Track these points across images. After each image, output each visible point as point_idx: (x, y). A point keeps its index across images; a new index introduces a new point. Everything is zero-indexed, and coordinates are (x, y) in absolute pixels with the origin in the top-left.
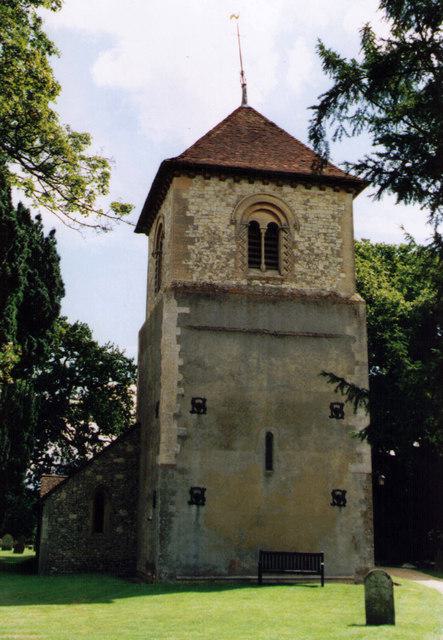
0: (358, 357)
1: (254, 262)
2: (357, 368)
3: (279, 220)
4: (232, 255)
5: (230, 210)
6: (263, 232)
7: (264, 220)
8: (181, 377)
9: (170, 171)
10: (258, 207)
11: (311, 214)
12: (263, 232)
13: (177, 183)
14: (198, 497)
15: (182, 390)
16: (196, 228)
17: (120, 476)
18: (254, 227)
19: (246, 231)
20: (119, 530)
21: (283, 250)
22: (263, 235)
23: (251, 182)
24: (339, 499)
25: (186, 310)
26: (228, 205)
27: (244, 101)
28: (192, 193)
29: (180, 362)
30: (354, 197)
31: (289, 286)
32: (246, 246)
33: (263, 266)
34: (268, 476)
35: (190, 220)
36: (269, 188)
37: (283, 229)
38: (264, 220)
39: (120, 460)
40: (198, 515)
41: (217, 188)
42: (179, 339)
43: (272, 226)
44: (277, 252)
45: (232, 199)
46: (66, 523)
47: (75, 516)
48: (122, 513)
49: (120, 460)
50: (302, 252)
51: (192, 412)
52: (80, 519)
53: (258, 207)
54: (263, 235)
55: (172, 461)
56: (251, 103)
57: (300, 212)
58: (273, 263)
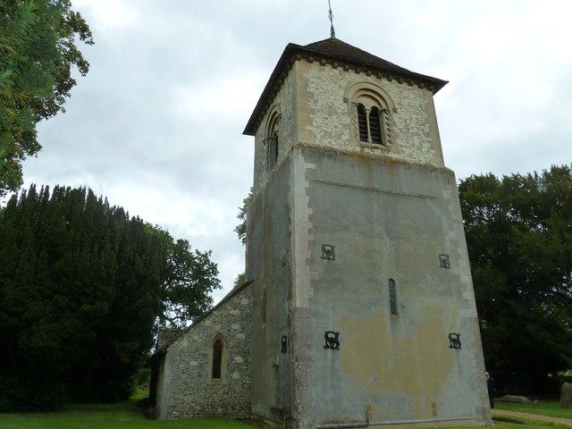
0: (454, 217)
1: (364, 138)
2: (455, 225)
3: (380, 104)
4: (345, 126)
5: (342, 92)
6: (368, 113)
7: (369, 104)
8: (311, 225)
9: (293, 54)
10: (363, 93)
11: (405, 102)
12: (368, 113)
13: (299, 65)
14: (332, 342)
15: (312, 237)
16: (316, 102)
17: (235, 326)
18: (361, 108)
19: (356, 108)
20: (236, 375)
21: (386, 127)
22: (368, 115)
23: (357, 72)
24: (455, 343)
25: (312, 166)
26: (340, 87)
27: (333, 33)
28: (311, 74)
29: (310, 212)
30: (434, 93)
31: (393, 156)
32: (357, 120)
33: (370, 139)
34: (393, 321)
35: (311, 95)
36: (372, 79)
37: (384, 111)
38: (369, 104)
39: (236, 312)
40: (333, 360)
41: (331, 73)
42: (309, 191)
43: (374, 109)
44: (379, 131)
45: (343, 83)
46: (187, 369)
47: (196, 364)
48: (239, 359)
49: (236, 312)
50: (401, 130)
51: (323, 258)
52: (201, 366)
53: (363, 93)
54: (368, 115)
55: (306, 305)
56: (337, 36)
57: (396, 100)
58: (378, 138)
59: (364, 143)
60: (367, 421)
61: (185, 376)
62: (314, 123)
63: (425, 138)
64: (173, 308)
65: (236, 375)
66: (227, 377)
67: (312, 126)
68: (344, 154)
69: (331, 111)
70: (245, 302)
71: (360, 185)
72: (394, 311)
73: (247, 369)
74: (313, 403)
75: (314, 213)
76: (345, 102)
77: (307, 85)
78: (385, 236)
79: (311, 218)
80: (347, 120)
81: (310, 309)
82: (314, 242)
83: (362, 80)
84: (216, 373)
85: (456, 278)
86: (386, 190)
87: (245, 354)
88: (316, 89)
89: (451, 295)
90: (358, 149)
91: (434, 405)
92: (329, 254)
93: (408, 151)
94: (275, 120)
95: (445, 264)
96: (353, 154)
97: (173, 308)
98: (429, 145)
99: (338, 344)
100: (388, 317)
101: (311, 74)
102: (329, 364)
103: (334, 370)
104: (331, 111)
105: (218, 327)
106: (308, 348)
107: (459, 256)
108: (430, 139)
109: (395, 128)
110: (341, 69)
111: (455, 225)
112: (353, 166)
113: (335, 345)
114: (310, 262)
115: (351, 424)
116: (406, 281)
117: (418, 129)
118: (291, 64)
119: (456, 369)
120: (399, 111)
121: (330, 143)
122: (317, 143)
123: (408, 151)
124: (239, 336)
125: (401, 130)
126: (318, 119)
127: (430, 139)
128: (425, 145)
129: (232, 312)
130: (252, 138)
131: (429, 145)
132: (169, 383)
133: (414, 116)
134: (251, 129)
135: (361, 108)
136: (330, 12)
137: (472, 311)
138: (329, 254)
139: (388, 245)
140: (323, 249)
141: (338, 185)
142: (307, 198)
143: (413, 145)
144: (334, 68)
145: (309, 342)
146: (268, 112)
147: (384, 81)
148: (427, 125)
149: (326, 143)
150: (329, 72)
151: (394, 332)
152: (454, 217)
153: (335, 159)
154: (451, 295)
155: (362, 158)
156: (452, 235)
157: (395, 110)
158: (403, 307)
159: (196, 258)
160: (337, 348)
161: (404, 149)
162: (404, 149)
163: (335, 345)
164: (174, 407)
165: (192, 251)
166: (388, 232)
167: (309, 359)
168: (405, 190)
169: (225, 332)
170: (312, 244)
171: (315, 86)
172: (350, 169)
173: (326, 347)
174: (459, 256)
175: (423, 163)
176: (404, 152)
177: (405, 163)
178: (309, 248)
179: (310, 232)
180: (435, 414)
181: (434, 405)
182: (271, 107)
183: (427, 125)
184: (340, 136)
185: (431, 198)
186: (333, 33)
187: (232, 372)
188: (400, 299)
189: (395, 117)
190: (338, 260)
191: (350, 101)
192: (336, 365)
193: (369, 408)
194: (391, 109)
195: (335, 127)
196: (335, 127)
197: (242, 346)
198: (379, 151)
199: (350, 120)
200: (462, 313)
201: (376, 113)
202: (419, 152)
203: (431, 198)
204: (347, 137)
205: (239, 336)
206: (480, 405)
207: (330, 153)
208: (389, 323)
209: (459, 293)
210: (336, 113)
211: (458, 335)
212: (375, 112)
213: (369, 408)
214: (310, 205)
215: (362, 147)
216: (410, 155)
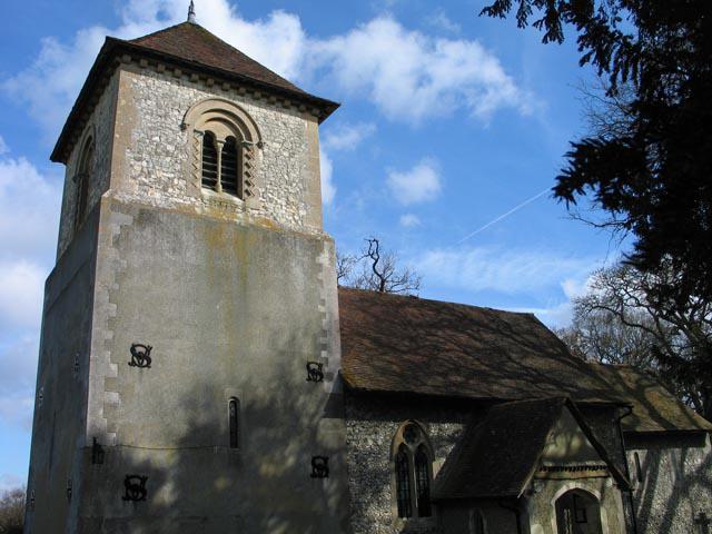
7: (222, 133)
18: (209, 138)
19: (201, 139)
27: (191, 12)
38: (222, 133)
56: (199, 20)
58: (233, 186)
94: (89, 147)
99: (149, 361)
113: (145, 362)
118: (115, 66)
130: (61, 168)
134: (60, 154)
135: (209, 138)
146: (84, 132)
157: (260, 145)
160: (148, 366)
163: (145, 362)
173: (132, 364)
186: (191, 12)
199: (258, 163)
201: (233, 147)
211: (149, 349)
212: (233, 147)
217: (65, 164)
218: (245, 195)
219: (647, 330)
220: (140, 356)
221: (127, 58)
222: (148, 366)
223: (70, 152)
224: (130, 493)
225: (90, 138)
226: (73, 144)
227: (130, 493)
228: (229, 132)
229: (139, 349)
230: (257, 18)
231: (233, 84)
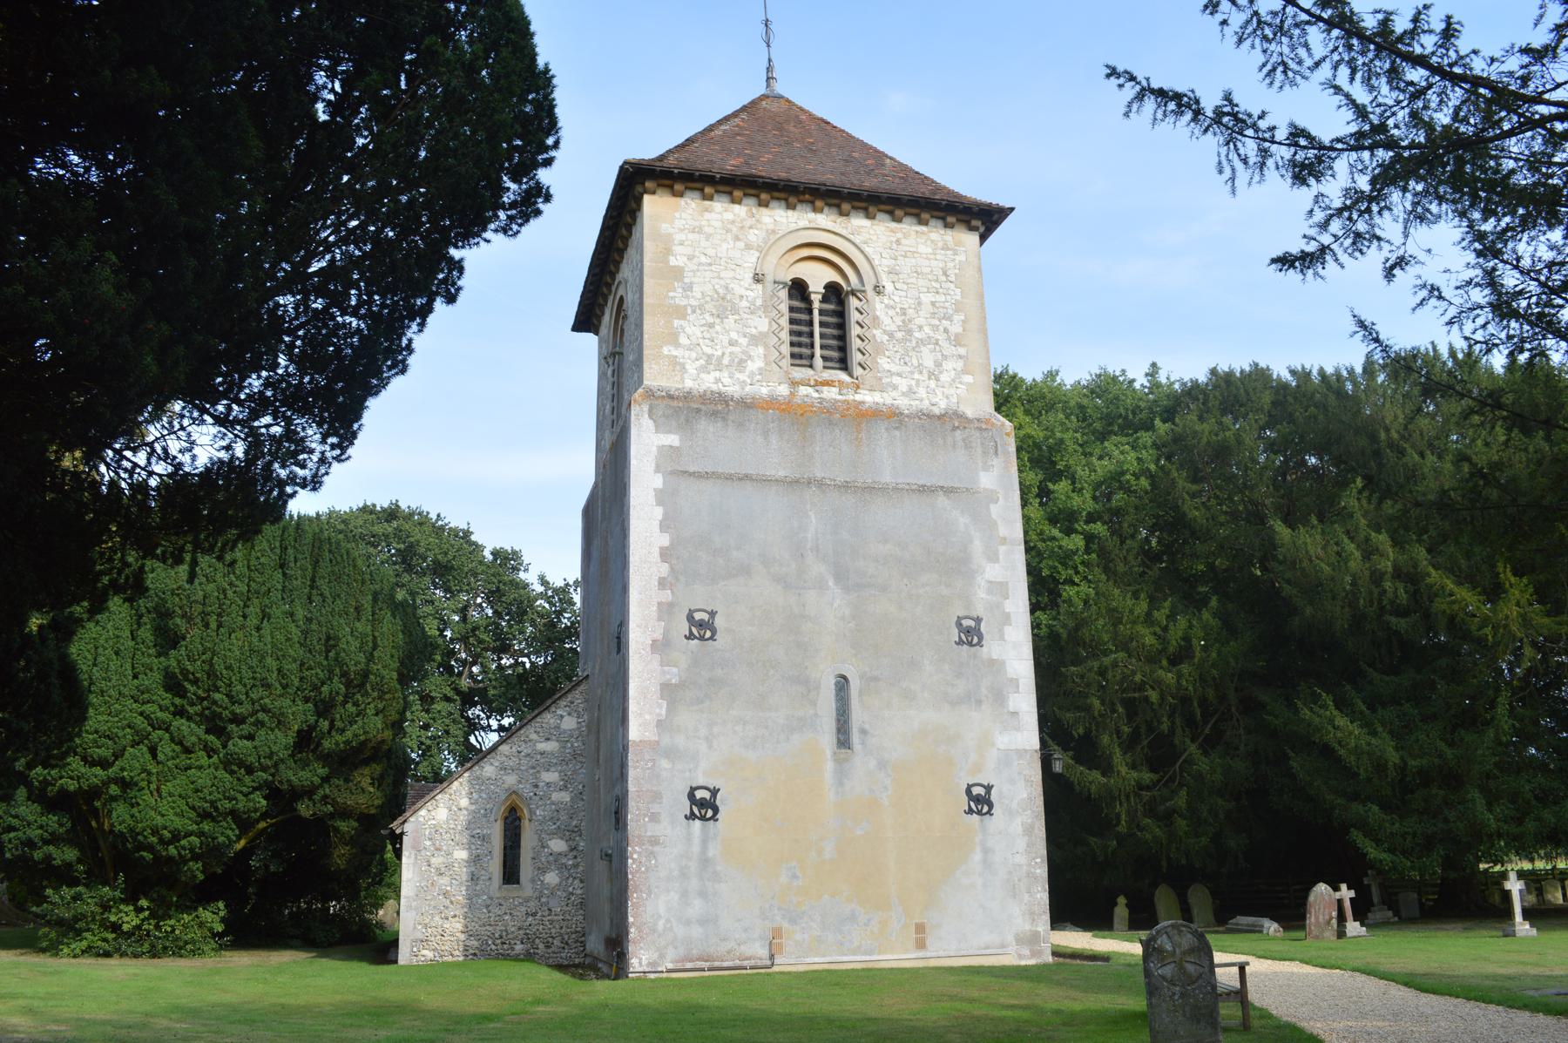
0: (1003, 531)
1: (801, 354)
2: (1002, 549)
4: (755, 340)
5: (751, 259)
6: (816, 299)
7: (818, 278)
11: (906, 265)
13: (655, 207)
14: (704, 806)
15: (667, 596)
16: (689, 288)
17: (551, 776)
18: (798, 289)
20: (552, 878)
24: (981, 802)
25: (673, 440)
26: (748, 247)
29: (665, 540)
31: (867, 397)
33: (818, 362)
34: (838, 761)
35: (678, 273)
37: (853, 293)
38: (818, 278)
40: (705, 842)
42: (661, 497)
45: (754, 236)
46: (449, 866)
48: (558, 845)
50: (891, 335)
55: (651, 735)
56: (780, 88)
57: (883, 264)
59: (800, 373)
60: (772, 957)
61: (444, 881)
62: (683, 340)
63: (949, 349)
64: (494, 724)
65: (552, 878)
66: (533, 881)
67: (677, 345)
68: (747, 405)
69: (724, 306)
70: (569, 723)
71: (782, 473)
72: (843, 738)
73: (576, 866)
74: (661, 925)
75: (672, 544)
76: (758, 281)
77: (668, 251)
78: (831, 583)
79: (665, 554)
80: (761, 324)
81: (658, 743)
82: (671, 605)
83: (802, 224)
84: (511, 874)
85: (996, 666)
86: (841, 479)
87: (570, 833)
88: (691, 258)
89: (1452, 619)
90: (783, 390)
91: (920, 928)
92: (702, 628)
93: (903, 384)
95: (971, 635)
96: (771, 403)
97: (494, 724)
98: (960, 365)
100: (829, 753)
101: (679, 223)
102: (696, 848)
103: (705, 862)
104: (724, 306)
105: (511, 780)
106: (650, 821)
107: (1007, 619)
108: (962, 351)
109: (877, 333)
110: (751, 201)
111: (1002, 549)
112: (766, 434)
114: (660, 647)
115: (738, 963)
116: (876, 679)
117: (935, 328)
119: (977, 856)
120: (889, 287)
121: (718, 381)
122: (689, 384)
123: (903, 384)
124: (556, 796)
125: (891, 335)
126: (691, 329)
127: (962, 351)
128: (949, 365)
129: (542, 746)
130: (589, 341)
131: (960, 365)
132: (411, 894)
133: (927, 298)
135: (798, 289)
136: (767, 23)
137: (1028, 736)
138: (702, 628)
139: (837, 602)
140: (690, 618)
141: (729, 478)
142: (659, 512)
143: (920, 368)
144: (733, 201)
145: (655, 808)
147: (858, 222)
148: (959, 318)
149: (709, 382)
150: (723, 213)
151: (840, 783)
152: (1003, 531)
153: (724, 419)
154: (979, 702)
155: (790, 414)
156: (992, 572)
157: (878, 290)
158: (863, 732)
159: (542, 595)
161: (896, 380)
162: (896, 380)
163: (986, 809)
164: (424, 941)
165: (530, 577)
166: (840, 576)
167: (655, 841)
168: (887, 478)
169: (526, 790)
170: (666, 610)
171: (689, 251)
172: (760, 439)
173: (692, 816)
174: (1007, 619)
175: (942, 405)
176: (895, 387)
177: (892, 416)
178: (660, 619)
179: (662, 583)
180: (921, 945)
181: (920, 928)
182: (614, 289)
183: (959, 318)
184: (741, 364)
185: (949, 491)
187: (543, 870)
188: (858, 716)
189: (879, 306)
190: (722, 639)
191: (769, 278)
192: (711, 854)
193: (777, 933)
194: (869, 288)
195: (732, 343)
196: (732, 343)
197: (564, 817)
198: (835, 390)
200: (1004, 741)
202: (932, 384)
203: (949, 491)
204: (760, 364)
205: (556, 796)
206: (1027, 927)
207: (715, 407)
208: (829, 766)
209: (999, 697)
210: (735, 311)
211: (989, 788)
212: (834, 293)
213: (777, 933)
214: (664, 526)
215: (794, 384)
216: (910, 392)
217: (596, 333)
218: (858, 371)
219: (1457, 489)
220: (703, 804)
221: (649, 184)
222: (714, 818)
223: (599, 318)
224: (695, 631)
225: (622, 298)
226: (602, 308)
227: (695, 631)
228: (831, 276)
229: (699, 794)
230: (378, 373)
231: (960, 217)
